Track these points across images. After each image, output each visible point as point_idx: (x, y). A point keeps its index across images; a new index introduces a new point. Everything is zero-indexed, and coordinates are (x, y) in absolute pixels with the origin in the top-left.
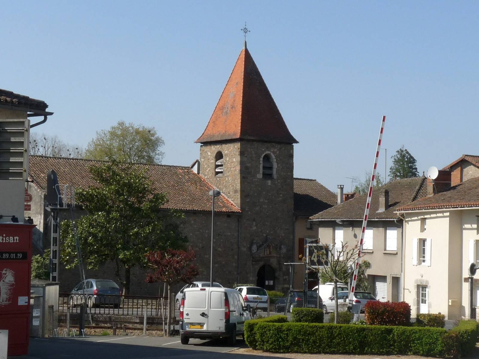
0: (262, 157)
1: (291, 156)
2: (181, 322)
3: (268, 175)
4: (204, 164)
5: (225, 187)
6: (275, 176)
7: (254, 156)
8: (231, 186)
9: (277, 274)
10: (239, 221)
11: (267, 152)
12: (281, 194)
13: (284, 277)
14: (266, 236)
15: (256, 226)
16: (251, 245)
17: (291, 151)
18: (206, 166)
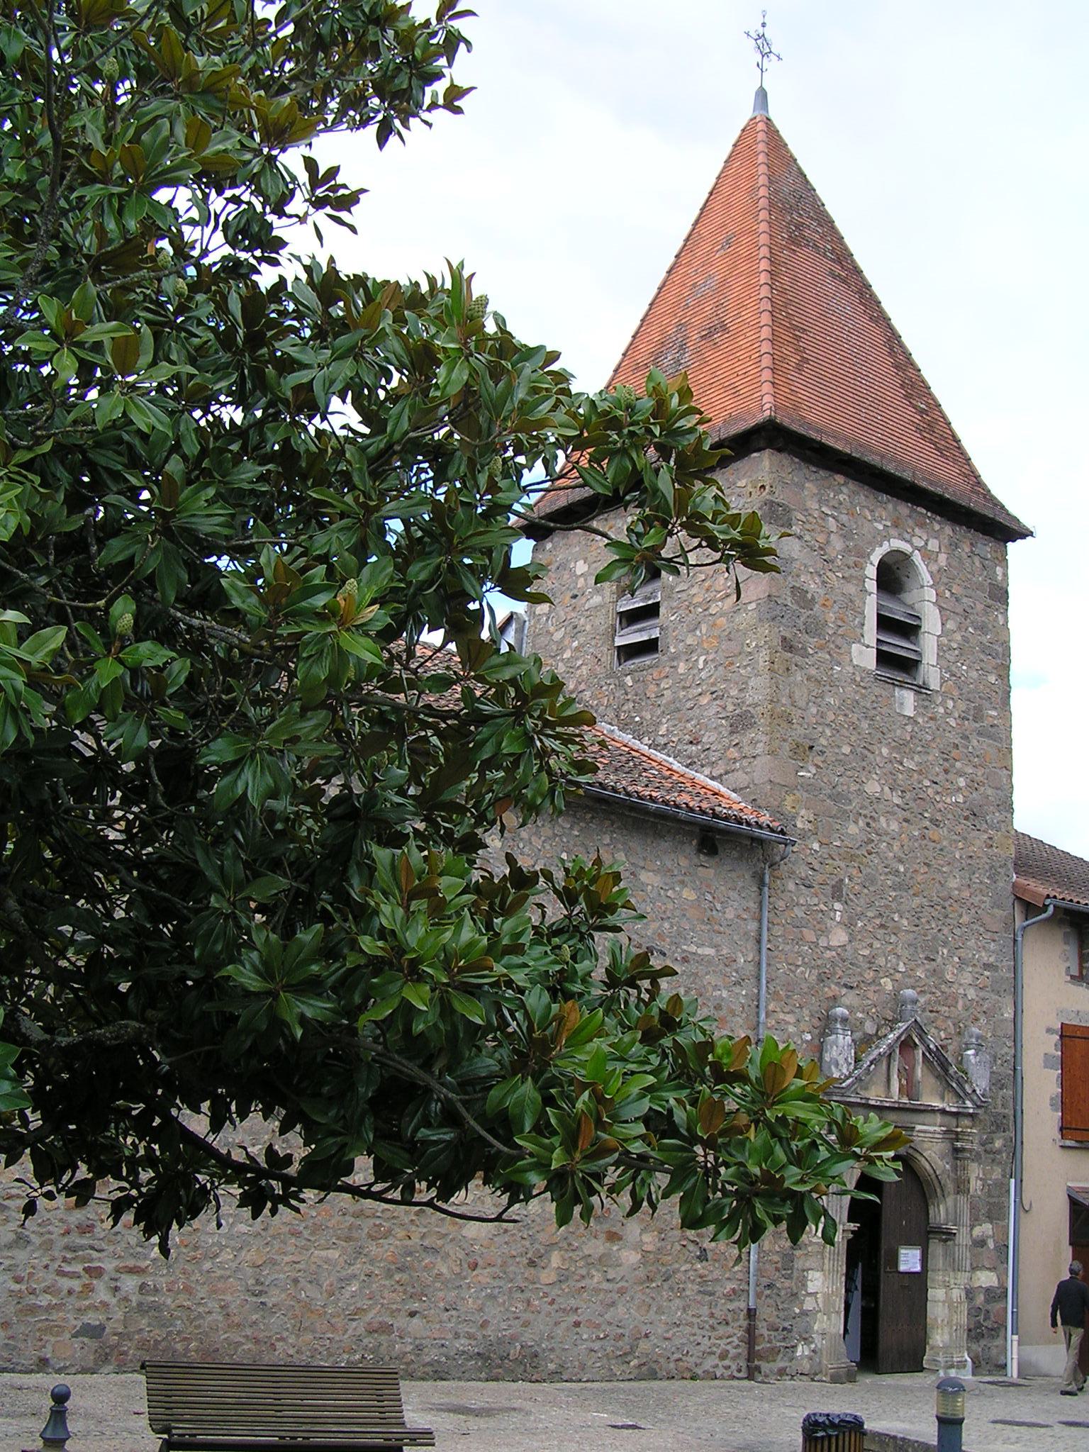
0: (876, 558)
1: (1000, 595)
2: (280, 821)
3: (898, 665)
4: (552, 629)
5: (674, 710)
6: (931, 672)
7: (837, 544)
8: (704, 700)
9: (940, 1213)
10: (761, 884)
11: (897, 544)
12: (960, 774)
13: (977, 1231)
14: (896, 994)
15: (849, 925)
16: (823, 1034)
17: (999, 570)
18: (558, 636)
